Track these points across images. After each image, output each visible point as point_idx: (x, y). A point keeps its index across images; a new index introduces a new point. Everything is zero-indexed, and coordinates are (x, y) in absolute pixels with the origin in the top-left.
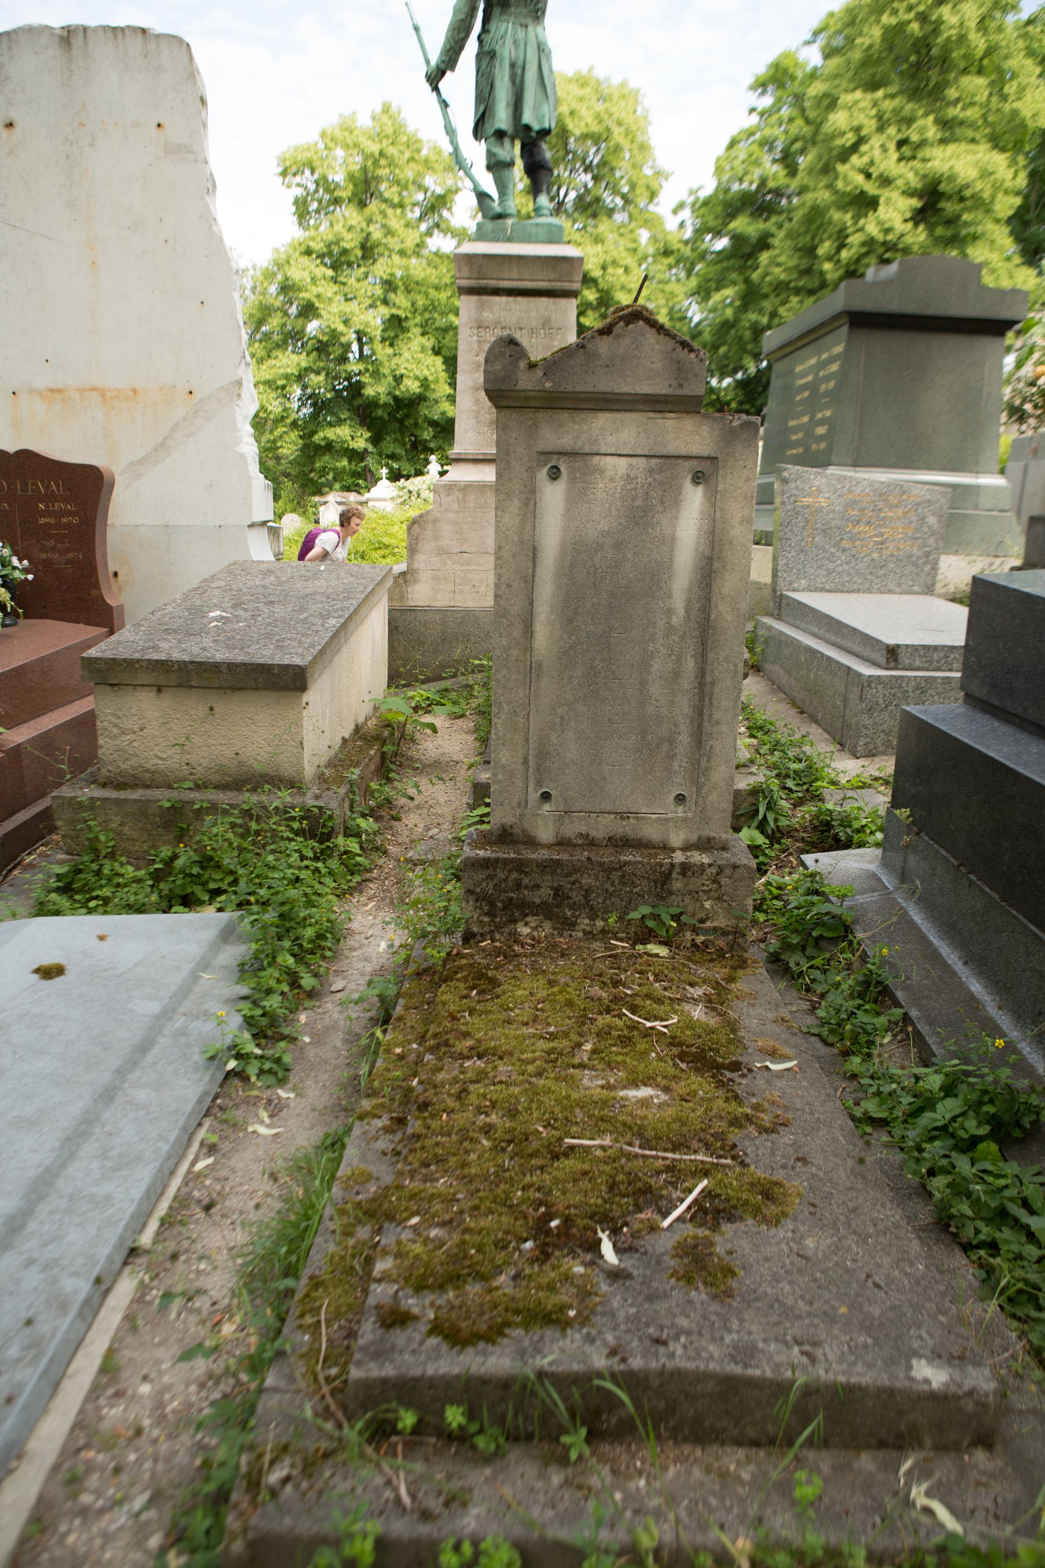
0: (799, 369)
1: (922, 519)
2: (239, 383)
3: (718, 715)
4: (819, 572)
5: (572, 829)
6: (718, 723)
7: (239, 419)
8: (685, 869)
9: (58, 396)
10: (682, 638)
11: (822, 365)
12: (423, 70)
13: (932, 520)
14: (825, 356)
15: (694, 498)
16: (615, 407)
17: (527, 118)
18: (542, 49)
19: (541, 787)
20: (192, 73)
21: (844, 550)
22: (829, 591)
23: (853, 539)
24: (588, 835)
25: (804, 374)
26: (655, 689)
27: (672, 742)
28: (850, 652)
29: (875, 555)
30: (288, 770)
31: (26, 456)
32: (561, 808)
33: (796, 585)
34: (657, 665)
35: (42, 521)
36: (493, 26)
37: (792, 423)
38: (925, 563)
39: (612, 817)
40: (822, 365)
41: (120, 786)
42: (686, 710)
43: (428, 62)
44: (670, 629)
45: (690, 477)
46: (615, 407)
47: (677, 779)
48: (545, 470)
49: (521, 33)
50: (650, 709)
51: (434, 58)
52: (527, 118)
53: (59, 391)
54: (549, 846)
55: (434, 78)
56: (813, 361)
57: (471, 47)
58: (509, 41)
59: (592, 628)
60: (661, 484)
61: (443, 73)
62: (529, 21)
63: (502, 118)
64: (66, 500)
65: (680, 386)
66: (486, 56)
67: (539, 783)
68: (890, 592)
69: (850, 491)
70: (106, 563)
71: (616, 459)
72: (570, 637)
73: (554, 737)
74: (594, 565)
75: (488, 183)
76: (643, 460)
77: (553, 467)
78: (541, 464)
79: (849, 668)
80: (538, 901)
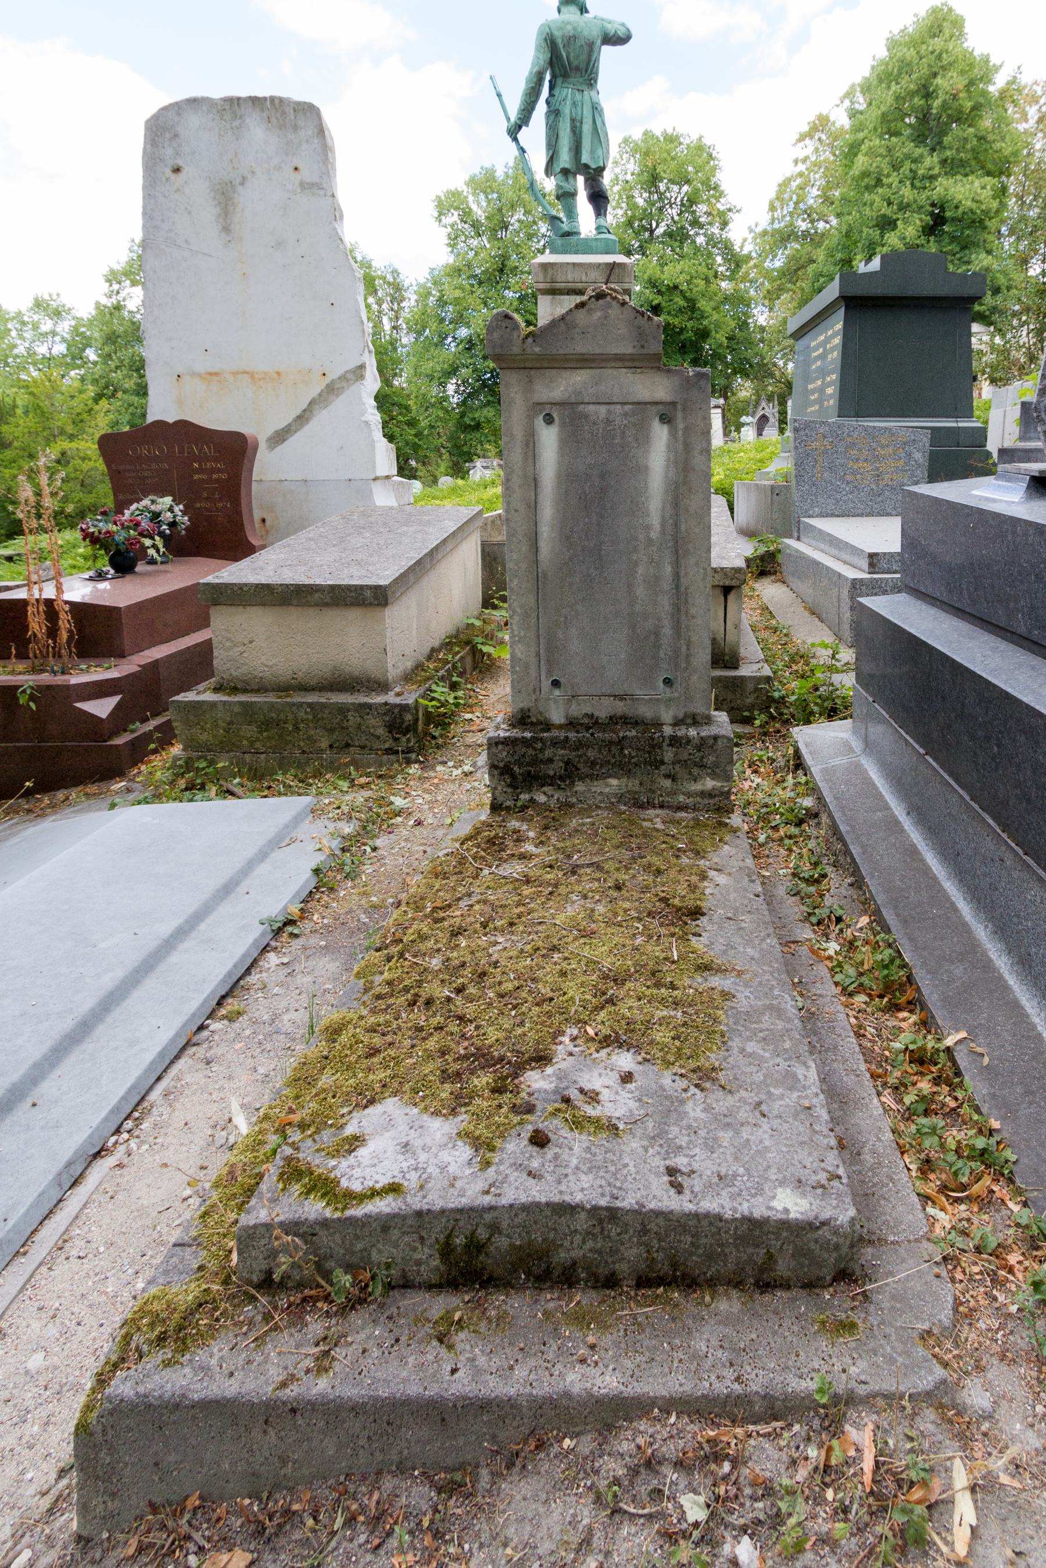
0: (813, 344)
1: (909, 455)
2: (362, 367)
3: (693, 611)
5: (577, 710)
6: (693, 617)
7: (364, 395)
8: (674, 741)
9: (215, 378)
11: (827, 340)
12: (505, 125)
14: (830, 333)
15: (660, 434)
17: (585, 158)
18: (596, 108)
20: (321, 131)
23: (854, 473)
25: (816, 348)
26: (640, 591)
27: (657, 634)
28: (845, 563)
29: (874, 486)
30: (376, 673)
31: (183, 425)
34: (640, 570)
35: (196, 477)
36: (556, 92)
37: (810, 387)
40: (827, 340)
41: (235, 690)
42: (667, 608)
43: (508, 119)
44: (650, 541)
47: (664, 665)
48: (541, 417)
49: (578, 97)
50: (637, 608)
51: (514, 116)
52: (585, 158)
53: (216, 374)
54: (560, 727)
55: (514, 132)
56: (822, 338)
57: (541, 108)
58: (569, 102)
60: (635, 425)
61: (520, 127)
62: (585, 87)
63: (565, 159)
64: (216, 460)
65: (643, 347)
66: (554, 113)
67: (549, 672)
69: (849, 435)
70: (251, 510)
71: (597, 407)
79: (840, 575)
80: (551, 773)
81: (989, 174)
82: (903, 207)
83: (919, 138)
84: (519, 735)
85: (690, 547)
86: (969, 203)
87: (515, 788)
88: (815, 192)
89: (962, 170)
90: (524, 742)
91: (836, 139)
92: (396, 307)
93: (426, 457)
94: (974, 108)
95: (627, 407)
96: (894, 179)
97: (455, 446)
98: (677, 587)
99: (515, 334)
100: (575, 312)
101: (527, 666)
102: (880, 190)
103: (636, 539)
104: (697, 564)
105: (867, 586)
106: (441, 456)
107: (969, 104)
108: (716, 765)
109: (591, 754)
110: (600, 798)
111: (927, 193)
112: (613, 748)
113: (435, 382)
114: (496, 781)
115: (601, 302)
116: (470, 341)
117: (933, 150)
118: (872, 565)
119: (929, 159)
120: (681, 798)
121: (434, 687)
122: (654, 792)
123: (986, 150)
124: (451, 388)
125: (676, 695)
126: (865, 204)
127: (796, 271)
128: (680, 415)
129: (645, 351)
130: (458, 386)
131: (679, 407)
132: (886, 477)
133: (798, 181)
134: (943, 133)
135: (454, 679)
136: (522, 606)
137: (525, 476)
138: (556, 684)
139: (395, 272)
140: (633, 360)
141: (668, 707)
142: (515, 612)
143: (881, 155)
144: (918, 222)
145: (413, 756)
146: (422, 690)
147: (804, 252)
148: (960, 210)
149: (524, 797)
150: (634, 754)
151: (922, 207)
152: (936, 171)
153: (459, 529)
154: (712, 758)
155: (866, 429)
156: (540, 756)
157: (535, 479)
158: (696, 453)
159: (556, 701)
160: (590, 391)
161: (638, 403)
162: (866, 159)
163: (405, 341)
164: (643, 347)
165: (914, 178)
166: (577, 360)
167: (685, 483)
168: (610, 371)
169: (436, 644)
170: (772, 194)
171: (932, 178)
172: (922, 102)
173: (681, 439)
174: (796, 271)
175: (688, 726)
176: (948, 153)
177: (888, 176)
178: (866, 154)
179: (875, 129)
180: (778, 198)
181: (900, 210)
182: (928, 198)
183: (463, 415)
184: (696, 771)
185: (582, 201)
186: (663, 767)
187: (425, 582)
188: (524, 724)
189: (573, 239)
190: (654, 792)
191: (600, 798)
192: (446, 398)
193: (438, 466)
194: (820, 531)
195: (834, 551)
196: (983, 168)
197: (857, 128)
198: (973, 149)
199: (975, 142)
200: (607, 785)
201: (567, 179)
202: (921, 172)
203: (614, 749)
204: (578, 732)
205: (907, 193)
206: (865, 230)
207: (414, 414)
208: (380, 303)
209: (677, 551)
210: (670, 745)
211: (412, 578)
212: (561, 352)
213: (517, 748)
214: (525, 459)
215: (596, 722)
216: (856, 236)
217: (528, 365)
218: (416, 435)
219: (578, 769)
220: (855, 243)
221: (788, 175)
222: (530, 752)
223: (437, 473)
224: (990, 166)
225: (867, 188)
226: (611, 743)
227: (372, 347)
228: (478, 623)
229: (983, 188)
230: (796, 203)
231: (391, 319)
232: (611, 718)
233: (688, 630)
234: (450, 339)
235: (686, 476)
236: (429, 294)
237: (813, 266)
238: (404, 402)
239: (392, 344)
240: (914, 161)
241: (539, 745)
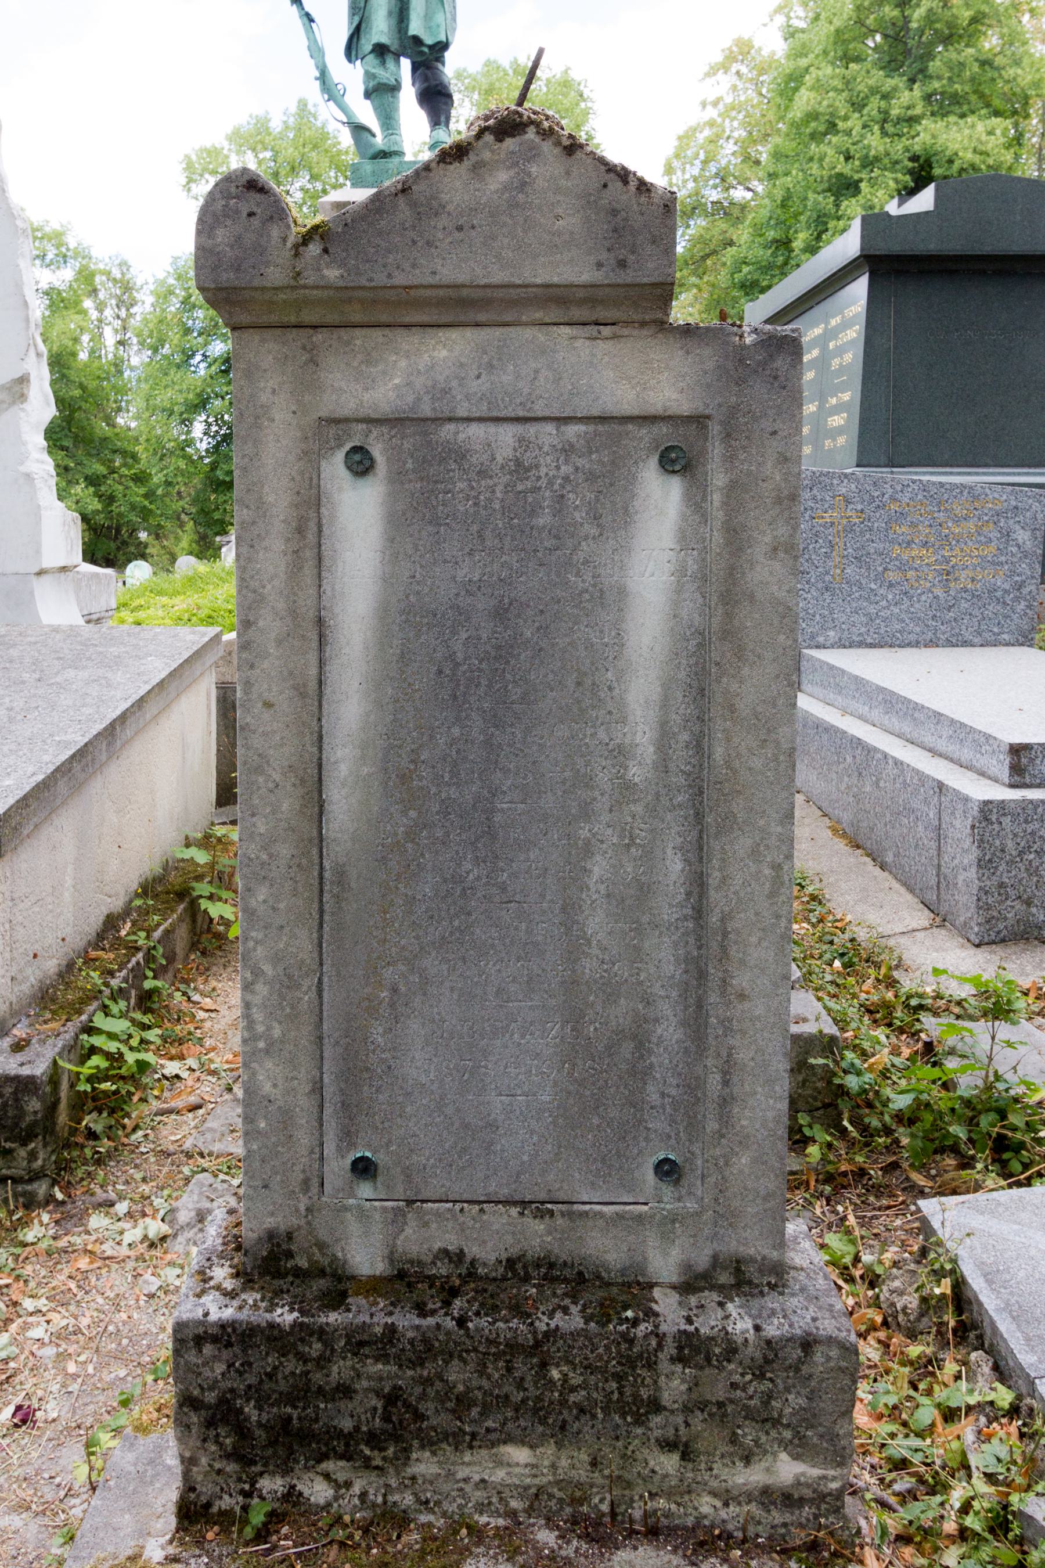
2: (23, 380)
3: (741, 980)
4: (855, 618)
6: (742, 996)
10: (652, 810)
13: (1023, 536)
16: (482, 317)
17: (415, 27)
19: (352, 1145)
21: (891, 585)
22: (871, 646)
24: (461, 1254)
27: (641, 1042)
28: (934, 752)
32: (400, 1192)
33: (821, 639)
34: (599, 868)
38: (1017, 599)
39: (514, 1211)
42: (669, 969)
45: (654, 461)
46: (482, 317)
47: (658, 1124)
48: (340, 456)
50: (589, 967)
52: (415, 27)
54: (374, 1286)
59: (453, 793)
60: (591, 477)
63: (380, 29)
65: (622, 264)
67: (348, 1137)
68: (966, 644)
69: (893, 499)
71: (492, 428)
72: (404, 813)
73: (377, 1033)
74: (451, 656)
75: (366, 114)
76: (550, 428)
77: (356, 449)
78: (326, 449)
79: (941, 786)
80: (347, 1424)
81: (997, 113)
82: (869, 163)
83: (891, 65)
84: (261, 1317)
85: (738, 806)
86: (969, 156)
87: (245, 1461)
88: (730, 147)
89: (957, 109)
90: (273, 1334)
91: (762, 71)
92: (123, 313)
93: (159, 526)
94: (974, 20)
95: (572, 431)
96: (854, 122)
97: (203, 511)
98: (699, 913)
99: (275, 232)
100: (439, 171)
101: (286, 1118)
102: (835, 139)
103: (588, 782)
104: (755, 853)
105: (1015, 816)
106: (182, 525)
107: (968, 14)
108: (808, 1418)
109: (458, 1375)
110: (479, 1495)
111: (905, 142)
112: (518, 1363)
113: (175, 418)
114: (194, 1442)
115: (510, 143)
116: (227, 360)
117: (912, 81)
118: (1016, 769)
119: (907, 93)
120: (706, 1505)
121: (100, 1021)
122: (629, 1485)
123: (993, 80)
124: (198, 429)
125: (691, 1205)
126: (811, 159)
127: (704, 258)
128: (716, 450)
129: (628, 277)
130: (209, 425)
131: (715, 428)
132: (963, 575)
133: (707, 132)
134: (929, 56)
135: (148, 984)
136: (276, 959)
137: (293, 613)
138: (363, 1168)
139: (124, 265)
140: (592, 302)
141: (667, 1238)
142: (257, 973)
143: (835, 89)
144: (892, 184)
145: (41, 1188)
146: (72, 1027)
147: (716, 232)
148: (956, 166)
149: (271, 1485)
150: (576, 1380)
151: (897, 162)
152: (918, 110)
153: (171, 675)
154: (796, 1400)
155: (925, 487)
156: (317, 1378)
157: (320, 622)
158: (759, 552)
159: (362, 1215)
160: (474, 386)
161: (602, 419)
162: (813, 95)
163: (135, 361)
164: (622, 264)
165: (885, 121)
166: (441, 303)
167: (727, 634)
168: (528, 333)
169: (117, 904)
170: (670, 151)
171: (912, 120)
172: (896, 13)
173: (718, 515)
174: (704, 258)
175: (727, 1292)
176: (936, 84)
177: (846, 118)
178: (812, 89)
179: (825, 52)
180: (677, 156)
181: (864, 166)
182: (907, 150)
183: (214, 466)
184: (748, 1434)
185: (408, 95)
186: (656, 1420)
187: (96, 786)
188: (279, 1274)
189: (396, 160)
190: (629, 1485)
191: (479, 1495)
192: (190, 443)
193: (178, 539)
194: (858, 682)
195: (895, 723)
196: (988, 105)
197: (800, 52)
198: (973, 79)
199: (976, 68)
200: (499, 1463)
201: (383, 63)
202: (895, 112)
203: (521, 1367)
204: (423, 1313)
205: (875, 142)
206: (811, 196)
207: (143, 464)
208: (100, 307)
209: (699, 816)
210: (679, 1359)
211: (62, 786)
212: (399, 279)
213: (253, 1355)
214: (295, 569)
215: (471, 1275)
216: (795, 206)
217: (309, 316)
218: (146, 496)
219: (419, 1417)
220: (796, 215)
221: (693, 122)
222: (292, 1365)
223: (177, 550)
224: (997, 102)
225: (813, 136)
226: (513, 1347)
227: (42, 348)
228: (202, 857)
229: (991, 133)
230: (705, 162)
231: (116, 331)
232: (511, 1263)
233: (728, 1031)
234: (198, 357)
235: (729, 616)
236: (171, 293)
237: (731, 251)
238: (130, 448)
239: (116, 365)
240: (885, 97)
241: (316, 1348)
